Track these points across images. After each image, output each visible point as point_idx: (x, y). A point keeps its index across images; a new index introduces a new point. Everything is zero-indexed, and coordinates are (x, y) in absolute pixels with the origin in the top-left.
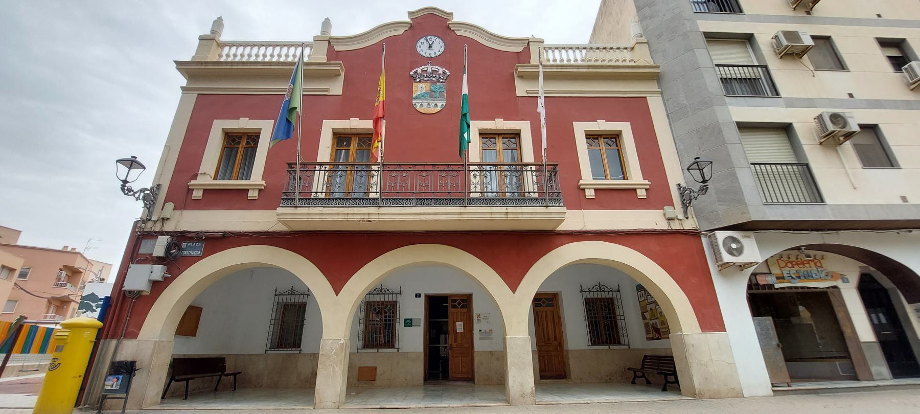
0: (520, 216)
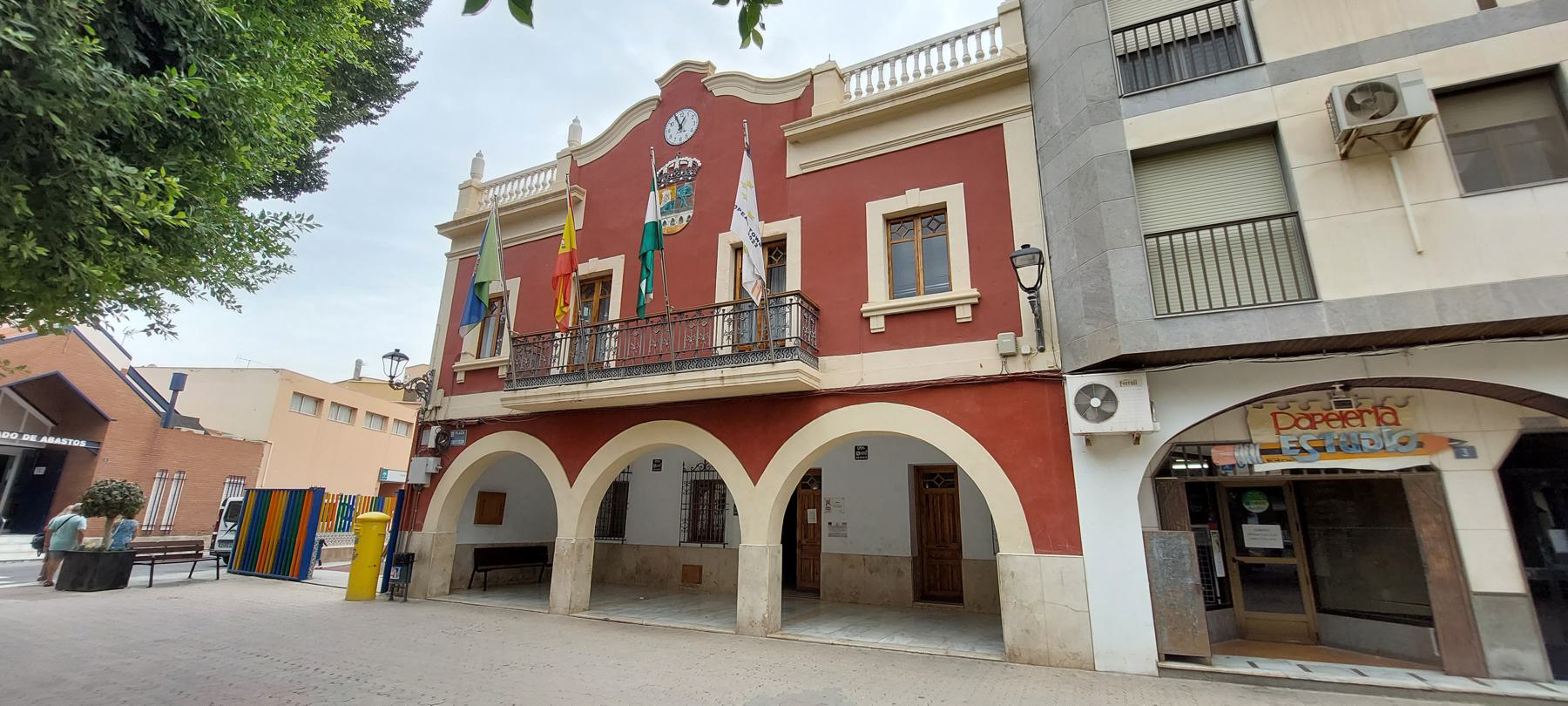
0: (738, 380)
